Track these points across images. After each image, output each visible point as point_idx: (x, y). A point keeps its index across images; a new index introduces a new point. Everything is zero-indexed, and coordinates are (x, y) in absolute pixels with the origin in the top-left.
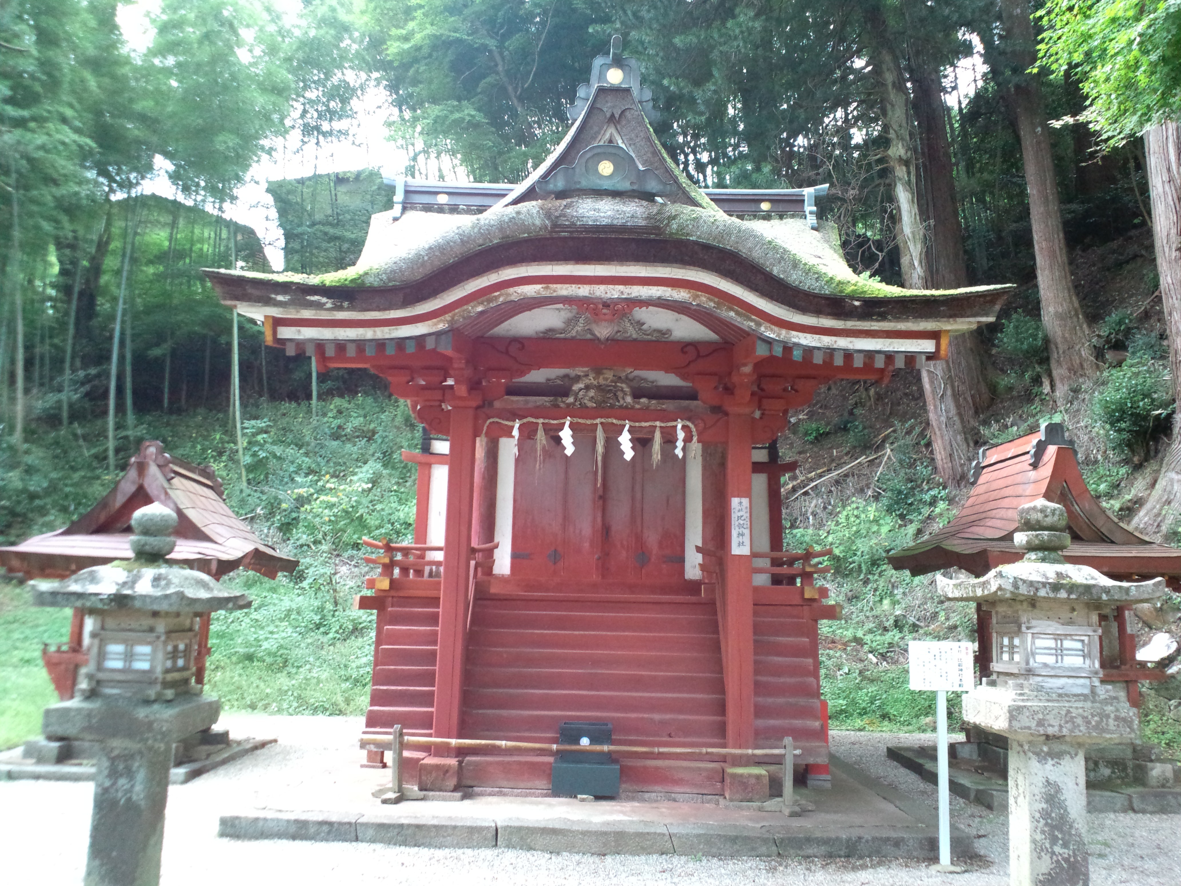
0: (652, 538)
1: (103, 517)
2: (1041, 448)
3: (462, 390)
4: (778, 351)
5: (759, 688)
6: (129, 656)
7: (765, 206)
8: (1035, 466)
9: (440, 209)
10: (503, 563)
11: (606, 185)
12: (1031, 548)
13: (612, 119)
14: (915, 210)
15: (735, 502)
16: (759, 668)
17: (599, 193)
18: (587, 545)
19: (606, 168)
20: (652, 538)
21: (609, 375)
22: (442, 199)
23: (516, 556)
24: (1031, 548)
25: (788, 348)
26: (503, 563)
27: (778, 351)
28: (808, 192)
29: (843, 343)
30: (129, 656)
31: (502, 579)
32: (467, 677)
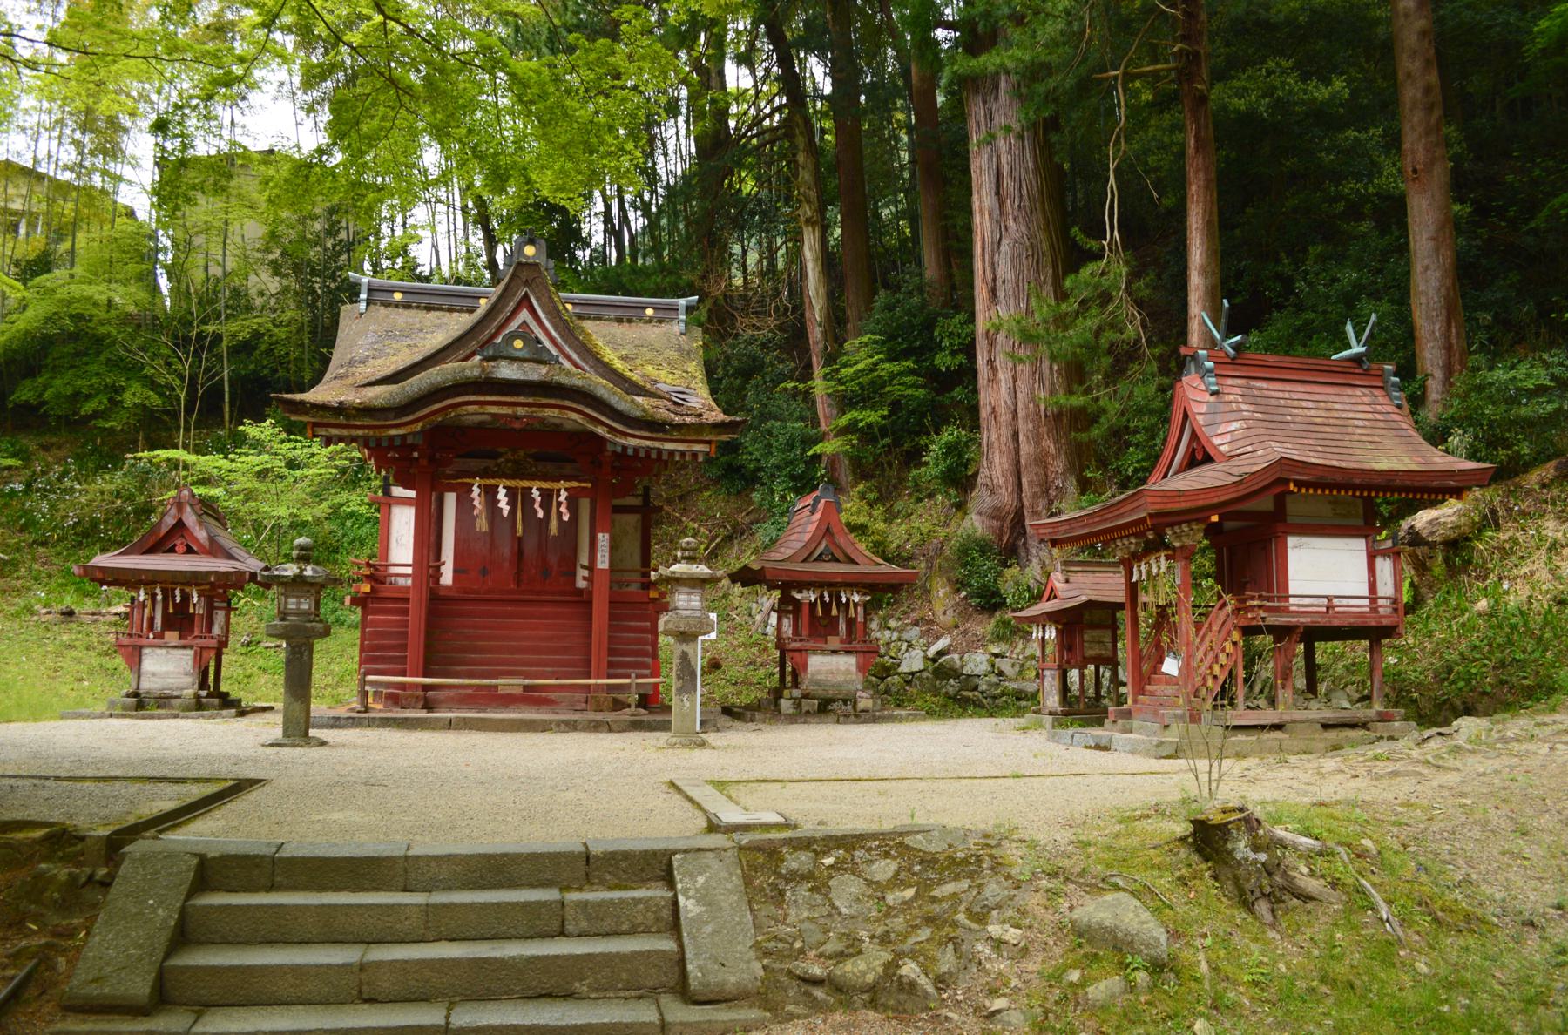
0: (553, 560)
1: (151, 541)
2: (817, 501)
3: (424, 462)
4: (619, 449)
5: (612, 652)
6: (299, 604)
7: (650, 312)
8: (812, 513)
9: (397, 305)
10: (447, 578)
11: (518, 354)
12: (684, 558)
13: (527, 283)
14: (819, 268)
15: (600, 536)
16: (611, 640)
17: (513, 359)
18: (506, 564)
19: (518, 344)
20: (553, 560)
21: (522, 453)
22: (398, 296)
23: (457, 571)
24: (684, 558)
25: (625, 448)
26: (447, 578)
27: (619, 449)
28: (682, 302)
29: (657, 444)
30: (299, 604)
31: (447, 588)
32: (428, 648)
